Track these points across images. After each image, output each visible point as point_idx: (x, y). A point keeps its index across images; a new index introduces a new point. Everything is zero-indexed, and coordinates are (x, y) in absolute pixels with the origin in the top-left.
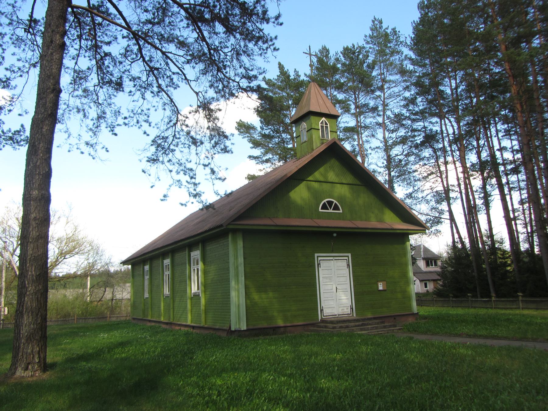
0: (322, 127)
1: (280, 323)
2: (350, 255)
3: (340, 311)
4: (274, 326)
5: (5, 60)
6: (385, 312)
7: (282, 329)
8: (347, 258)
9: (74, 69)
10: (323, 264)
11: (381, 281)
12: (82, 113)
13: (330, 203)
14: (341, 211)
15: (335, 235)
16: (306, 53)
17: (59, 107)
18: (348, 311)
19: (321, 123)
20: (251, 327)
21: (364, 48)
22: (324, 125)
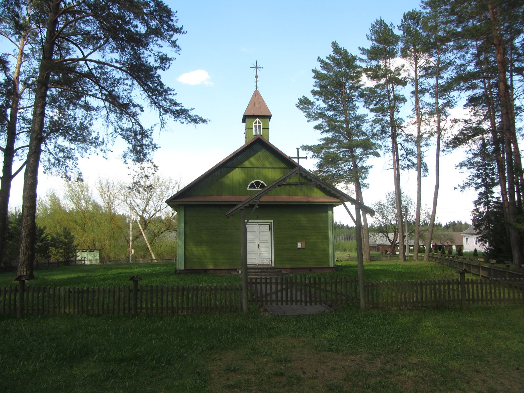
1: (211, 267)
2: (272, 221)
3: (261, 261)
4: (206, 268)
5: (168, 70)
6: (302, 265)
7: (211, 272)
8: (270, 224)
9: (105, 106)
11: (300, 241)
13: (258, 184)
14: (248, 189)
16: (253, 68)
17: (13, 160)
18: (268, 262)
19: (255, 123)
20: (188, 268)
21: (421, 13)
22: (258, 124)
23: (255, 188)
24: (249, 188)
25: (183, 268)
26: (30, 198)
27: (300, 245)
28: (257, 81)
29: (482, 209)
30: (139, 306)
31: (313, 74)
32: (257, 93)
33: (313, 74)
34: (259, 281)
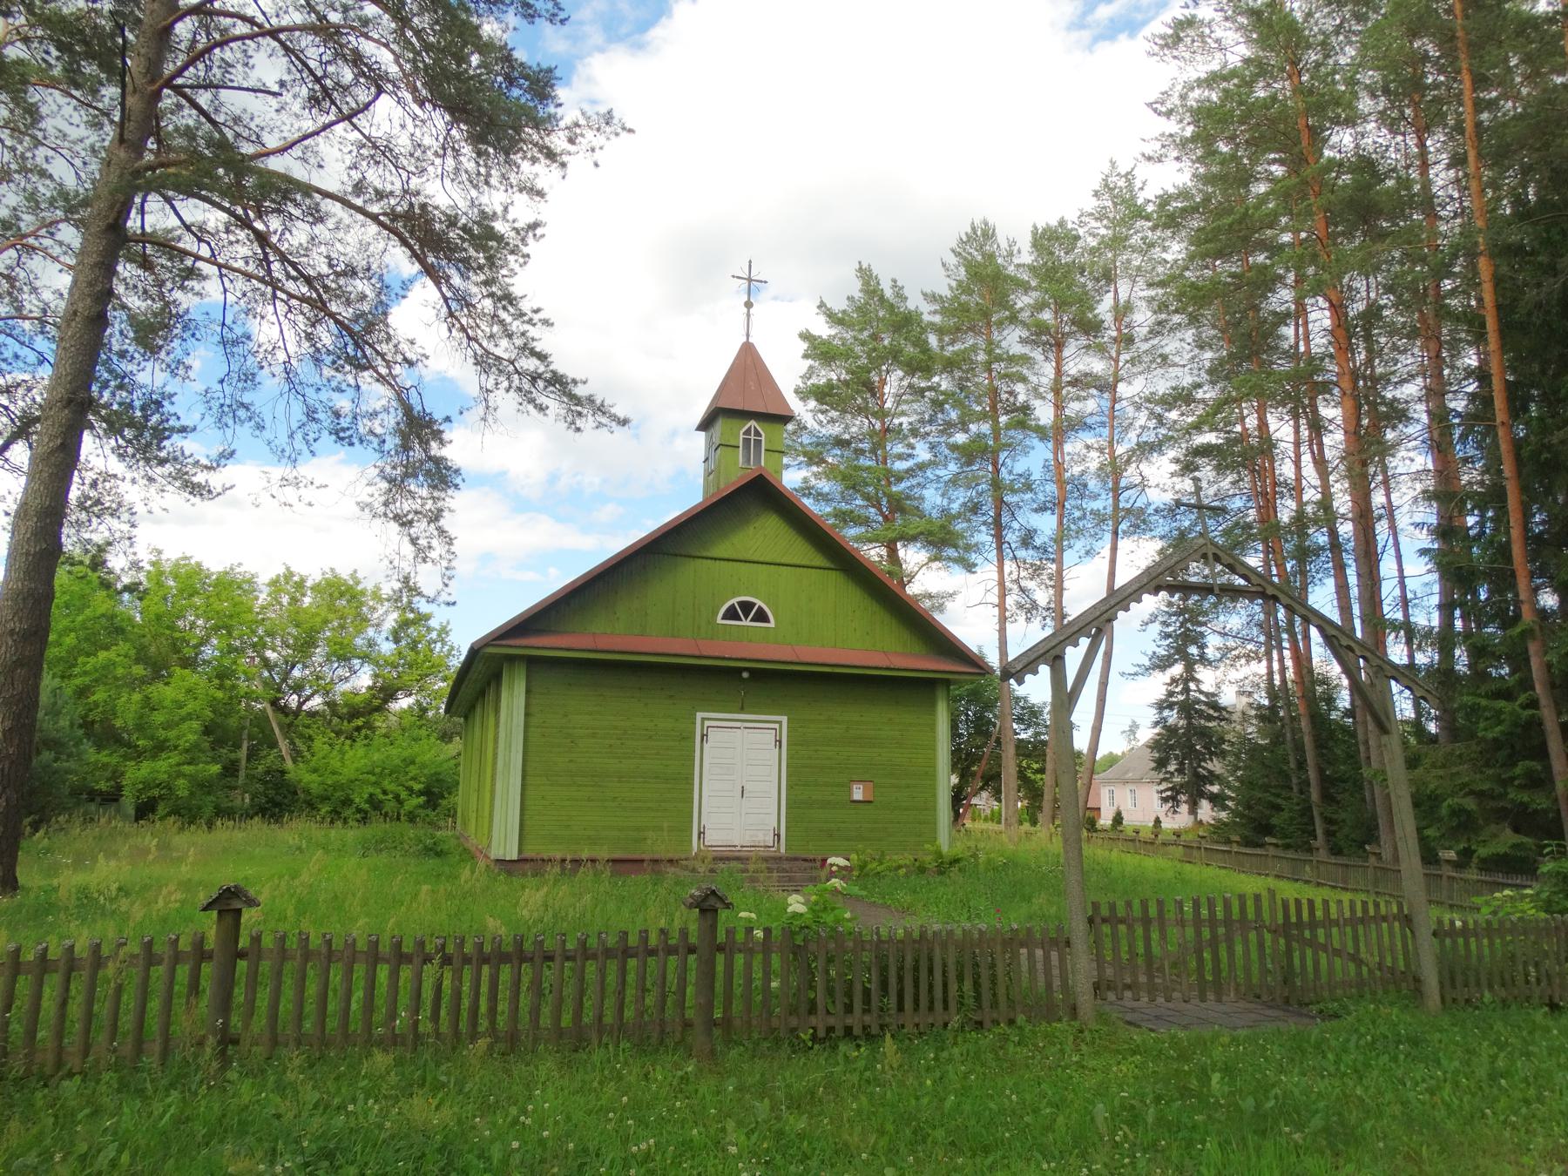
0: (747, 441)
2: (784, 719)
10: (713, 735)
12: (276, 88)
13: (747, 607)
14: (719, 621)
15: (745, 675)
20: (527, 854)
23: (738, 618)
24: (725, 617)
25: (515, 857)
26: (30, 602)
27: (858, 793)
28: (748, 315)
29: (1172, 717)
30: (718, 1014)
31: (805, 345)
32: (748, 351)
33: (805, 345)
34: (1121, 912)
